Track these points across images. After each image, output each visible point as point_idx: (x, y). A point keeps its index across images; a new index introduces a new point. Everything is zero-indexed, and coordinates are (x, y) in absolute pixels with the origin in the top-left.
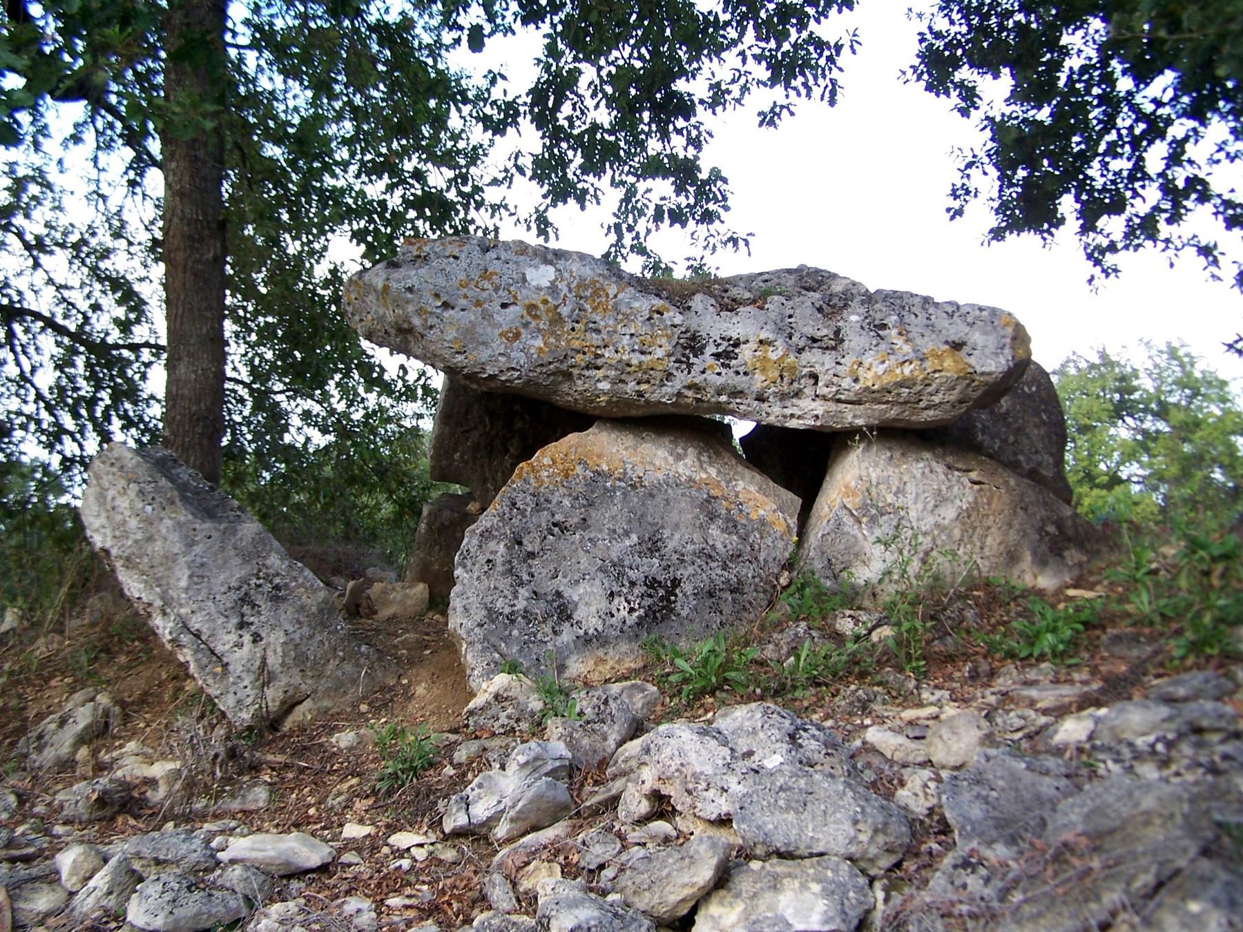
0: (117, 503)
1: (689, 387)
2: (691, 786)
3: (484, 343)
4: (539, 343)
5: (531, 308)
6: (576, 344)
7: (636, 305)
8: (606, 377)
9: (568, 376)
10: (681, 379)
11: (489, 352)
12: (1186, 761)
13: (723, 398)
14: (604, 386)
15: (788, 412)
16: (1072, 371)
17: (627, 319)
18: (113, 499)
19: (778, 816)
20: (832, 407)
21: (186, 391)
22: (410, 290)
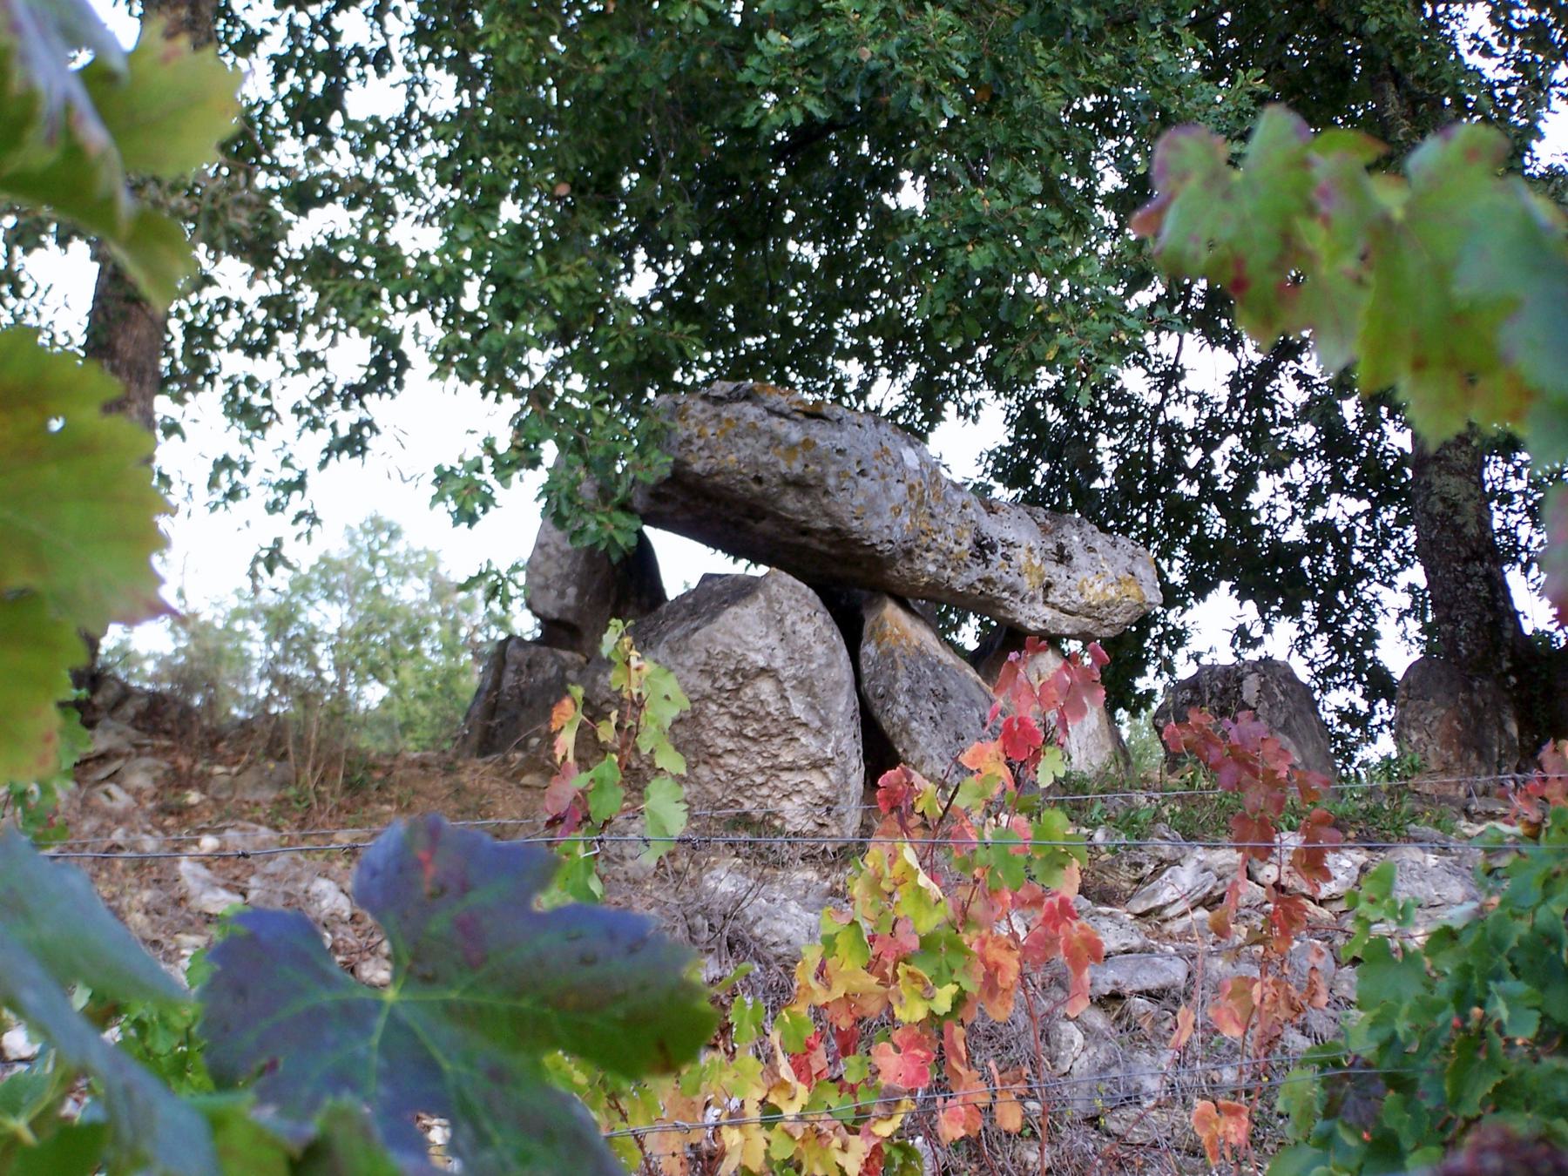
0: (798, 628)
4: (907, 521)
6: (924, 526)
8: (935, 561)
9: (908, 553)
10: (977, 572)
13: (1006, 595)
14: (932, 568)
15: (1033, 613)
17: (949, 510)
18: (793, 624)
20: (1056, 613)
22: (840, 452)
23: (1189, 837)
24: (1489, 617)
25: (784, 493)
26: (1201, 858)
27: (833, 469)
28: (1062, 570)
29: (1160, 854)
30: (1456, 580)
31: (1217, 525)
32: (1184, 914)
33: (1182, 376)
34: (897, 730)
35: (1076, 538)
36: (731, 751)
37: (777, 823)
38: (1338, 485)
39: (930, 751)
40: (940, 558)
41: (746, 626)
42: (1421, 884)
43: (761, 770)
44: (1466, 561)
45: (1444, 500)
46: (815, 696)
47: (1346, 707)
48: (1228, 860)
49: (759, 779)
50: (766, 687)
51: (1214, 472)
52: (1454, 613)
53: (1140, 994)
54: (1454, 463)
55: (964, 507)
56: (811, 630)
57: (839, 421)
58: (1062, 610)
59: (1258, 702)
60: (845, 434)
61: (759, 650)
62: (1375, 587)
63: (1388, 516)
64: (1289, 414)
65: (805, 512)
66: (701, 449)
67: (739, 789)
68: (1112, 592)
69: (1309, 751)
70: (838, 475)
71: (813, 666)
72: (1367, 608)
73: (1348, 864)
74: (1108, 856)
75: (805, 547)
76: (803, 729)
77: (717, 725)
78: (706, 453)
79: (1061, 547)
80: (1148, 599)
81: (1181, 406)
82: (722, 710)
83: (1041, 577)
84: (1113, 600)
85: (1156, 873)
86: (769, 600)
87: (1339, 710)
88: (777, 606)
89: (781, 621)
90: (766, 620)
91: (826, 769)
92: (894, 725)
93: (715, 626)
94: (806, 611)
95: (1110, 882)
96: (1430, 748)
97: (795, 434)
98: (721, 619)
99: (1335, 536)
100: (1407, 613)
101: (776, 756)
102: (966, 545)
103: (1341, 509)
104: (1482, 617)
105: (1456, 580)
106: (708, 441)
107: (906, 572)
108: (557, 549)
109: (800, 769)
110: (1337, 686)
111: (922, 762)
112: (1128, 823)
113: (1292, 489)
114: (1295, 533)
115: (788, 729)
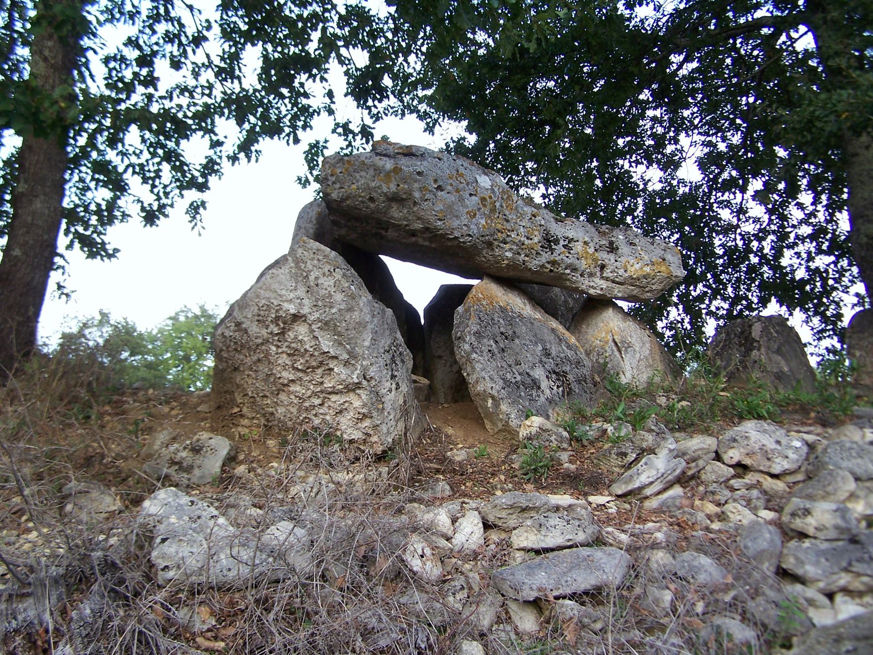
0: (320, 282)
1: (548, 262)
2: (770, 456)
3: (457, 216)
4: (483, 222)
5: (483, 199)
6: (499, 226)
7: (525, 209)
9: (490, 245)
10: (545, 257)
11: (458, 222)
13: (568, 271)
14: (509, 254)
15: (592, 284)
16: (182, 319)
17: (521, 216)
18: (317, 278)
19: (854, 461)
20: (610, 284)
21: (40, 223)
22: (419, 173)
25: (390, 207)
26: (672, 447)
27: (416, 185)
28: (612, 257)
31: (767, 272)
32: (659, 493)
33: (746, 212)
34: (464, 360)
35: (621, 237)
36: (293, 381)
37: (339, 433)
38: (819, 251)
40: (515, 247)
41: (280, 283)
42: (859, 461)
43: (315, 394)
45: (867, 236)
46: (340, 334)
47: (830, 347)
49: (317, 402)
50: (301, 330)
51: (765, 252)
53: (573, 596)
56: (332, 283)
57: (422, 155)
58: (613, 282)
59: (761, 337)
60: (425, 163)
62: (841, 294)
63: (844, 263)
64: (795, 223)
65: (405, 219)
66: (334, 183)
68: (647, 269)
71: (334, 311)
72: (837, 304)
73: (798, 444)
75: (416, 244)
76: (335, 362)
78: (338, 186)
80: (674, 274)
81: (747, 223)
84: (648, 274)
85: (637, 460)
87: (827, 349)
90: (295, 277)
91: (358, 391)
92: (462, 356)
94: (327, 268)
96: (868, 359)
97: (389, 165)
99: (820, 273)
101: (322, 383)
102: (536, 240)
103: (821, 261)
106: (338, 177)
110: (825, 338)
111: (477, 382)
113: (798, 255)
115: (323, 362)
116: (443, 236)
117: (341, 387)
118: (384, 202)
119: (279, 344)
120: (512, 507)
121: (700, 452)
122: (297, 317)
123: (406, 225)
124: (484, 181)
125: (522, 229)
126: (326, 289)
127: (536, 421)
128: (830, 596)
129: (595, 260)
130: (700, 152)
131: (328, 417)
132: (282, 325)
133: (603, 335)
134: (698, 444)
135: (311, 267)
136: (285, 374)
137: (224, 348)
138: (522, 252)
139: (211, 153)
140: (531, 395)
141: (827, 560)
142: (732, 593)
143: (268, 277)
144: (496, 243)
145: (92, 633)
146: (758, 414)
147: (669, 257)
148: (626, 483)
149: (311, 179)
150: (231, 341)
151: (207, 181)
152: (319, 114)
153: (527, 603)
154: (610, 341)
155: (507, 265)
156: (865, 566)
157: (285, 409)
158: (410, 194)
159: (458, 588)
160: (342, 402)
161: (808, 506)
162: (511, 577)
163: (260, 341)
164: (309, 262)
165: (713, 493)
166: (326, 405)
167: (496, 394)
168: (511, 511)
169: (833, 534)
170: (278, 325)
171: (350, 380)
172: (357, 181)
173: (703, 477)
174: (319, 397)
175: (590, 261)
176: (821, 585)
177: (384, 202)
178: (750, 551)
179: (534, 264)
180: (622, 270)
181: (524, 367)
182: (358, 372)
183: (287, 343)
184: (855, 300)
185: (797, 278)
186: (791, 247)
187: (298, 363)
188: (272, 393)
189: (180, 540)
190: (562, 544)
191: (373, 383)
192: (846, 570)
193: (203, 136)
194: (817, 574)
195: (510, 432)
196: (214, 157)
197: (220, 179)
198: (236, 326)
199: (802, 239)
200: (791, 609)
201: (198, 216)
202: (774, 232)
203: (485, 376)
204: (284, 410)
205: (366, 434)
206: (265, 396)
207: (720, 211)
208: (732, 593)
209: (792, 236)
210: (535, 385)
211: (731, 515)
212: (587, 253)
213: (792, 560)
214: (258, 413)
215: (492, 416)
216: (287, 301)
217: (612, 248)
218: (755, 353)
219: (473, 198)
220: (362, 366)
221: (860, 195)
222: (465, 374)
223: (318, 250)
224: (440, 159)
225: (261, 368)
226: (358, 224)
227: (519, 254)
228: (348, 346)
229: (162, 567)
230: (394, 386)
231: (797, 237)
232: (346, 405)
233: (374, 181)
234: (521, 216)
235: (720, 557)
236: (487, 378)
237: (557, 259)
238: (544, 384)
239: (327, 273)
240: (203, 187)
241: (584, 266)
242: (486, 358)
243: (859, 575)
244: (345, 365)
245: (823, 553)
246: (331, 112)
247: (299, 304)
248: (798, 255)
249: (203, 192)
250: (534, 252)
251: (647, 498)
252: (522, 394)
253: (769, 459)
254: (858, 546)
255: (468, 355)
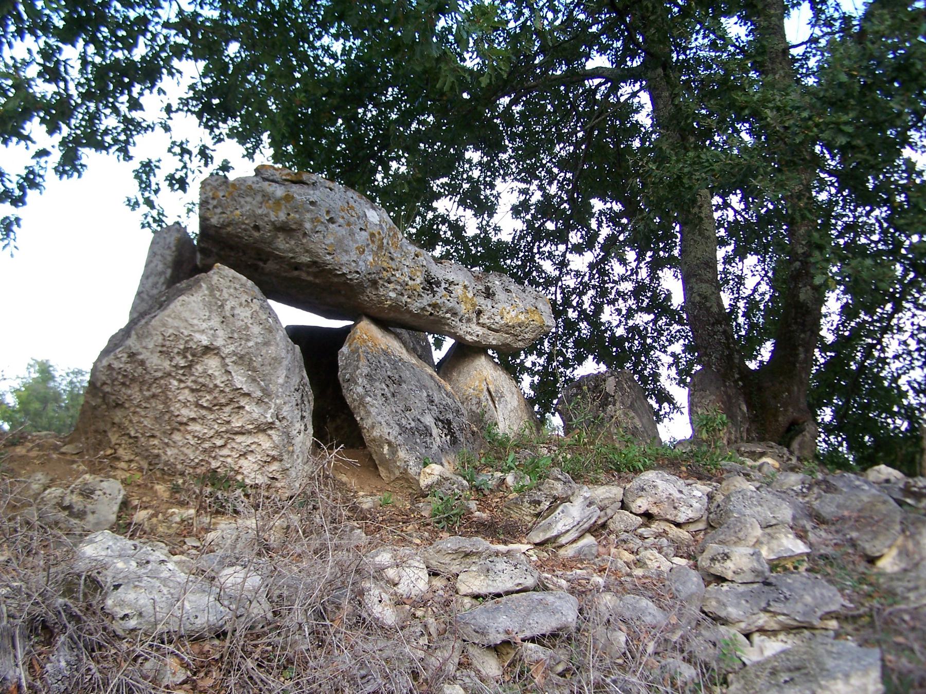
0: (236, 312)
1: (429, 305)
4: (370, 259)
6: (385, 265)
7: (409, 248)
8: (395, 289)
9: (374, 283)
10: (427, 299)
12: (815, 496)
13: (448, 315)
14: (393, 295)
15: (469, 330)
17: (405, 255)
18: (233, 308)
19: (756, 509)
22: (312, 203)
23: (577, 477)
24: (726, 353)
25: (276, 237)
27: (308, 216)
28: (489, 302)
29: (555, 493)
30: (709, 334)
32: (574, 541)
33: (568, 265)
34: (356, 404)
35: (497, 282)
36: (194, 419)
37: (239, 477)
38: (640, 309)
39: (379, 418)
40: (399, 288)
41: (192, 311)
42: (759, 508)
43: (218, 434)
44: (713, 325)
45: (699, 295)
46: (254, 370)
48: (608, 495)
50: (212, 364)
51: (584, 307)
52: (708, 351)
53: (533, 640)
54: (704, 277)
55: (417, 256)
56: (248, 314)
57: (313, 184)
58: (489, 328)
60: (317, 192)
61: (203, 332)
64: (616, 278)
65: (292, 250)
66: (215, 207)
67: (205, 451)
68: (522, 317)
69: (645, 420)
70: (312, 221)
71: (251, 344)
72: (655, 363)
74: (514, 495)
75: (298, 279)
76: (247, 399)
77: (180, 398)
78: (219, 210)
79: (488, 288)
80: (546, 324)
81: (569, 277)
82: (182, 385)
83: (474, 305)
84: (523, 322)
85: (551, 509)
86: (211, 289)
88: (218, 294)
89: (222, 306)
90: (209, 306)
91: (269, 432)
92: (354, 400)
93: (167, 312)
94: (244, 297)
95: (515, 516)
97: (280, 192)
98: (172, 306)
99: (639, 333)
100: (672, 365)
101: (228, 422)
102: (418, 281)
103: (642, 319)
104: (723, 352)
105: (709, 334)
107: (374, 297)
108: (148, 295)
109: (249, 432)
111: (373, 427)
112: (534, 469)
113: (619, 311)
114: (620, 332)
115: (234, 399)
116: (331, 272)
117: (251, 427)
118: (270, 231)
119: (183, 378)
120: (456, 552)
121: (606, 502)
122: (208, 350)
123: (292, 258)
124: (373, 216)
125: (406, 269)
126: (242, 321)
127: (435, 470)
128: (748, 636)
129: (474, 305)
130: (516, 199)
131: (229, 460)
132: (190, 358)
133: (477, 383)
134: (604, 493)
135: (226, 296)
136: (185, 412)
137: (109, 382)
138: (405, 293)
139: (33, 163)
140: (426, 442)
141: (747, 601)
142: (679, 633)
143: (178, 304)
144: (381, 282)
145: (70, 688)
146: (634, 467)
147: (540, 306)
148: (544, 531)
149: (141, 201)
150: (119, 373)
151: (25, 194)
152: (153, 129)
153: (489, 647)
154: (485, 389)
155: (390, 305)
156: (782, 605)
157: (181, 450)
158: (301, 225)
159: (418, 634)
160: (249, 442)
161: (726, 551)
162: (473, 621)
163: (159, 374)
164: (225, 290)
165: (625, 541)
166: (229, 446)
167: (393, 440)
168: (454, 557)
169: (749, 577)
170: (185, 357)
171: (263, 420)
172: (242, 207)
173: (612, 526)
174: (222, 437)
175: (469, 306)
176: (743, 625)
177: (270, 231)
178: (682, 594)
179: (415, 306)
180: (499, 317)
181: (415, 413)
182: (272, 410)
183: (193, 378)
184: (671, 360)
185: (617, 335)
186: (612, 302)
187: (204, 400)
188: (165, 433)
189: (136, 586)
190: (511, 589)
191: (285, 423)
192: (765, 610)
193: (17, 143)
194: (739, 615)
195: (407, 480)
196: (37, 169)
197: (41, 193)
198: (129, 357)
199: (621, 295)
200: (726, 651)
201: (12, 234)
202: (594, 287)
203: (379, 420)
204: (176, 451)
205: (273, 478)
206: (153, 436)
207: (542, 262)
208: (679, 633)
209: (614, 292)
210: (427, 432)
211: (648, 562)
212: (467, 297)
213: (714, 603)
214: (137, 455)
215: (388, 464)
216: (199, 331)
217: (489, 294)
218: (610, 407)
219: (363, 233)
220: (275, 404)
221: (693, 254)
222: (358, 419)
223: (234, 278)
224: (331, 189)
225: (154, 405)
226: (232, 254)
227: (402, 294)
228: (262, 383)
229: (121, 615)
230: (303, 428)
231: (618, 293)
232: (253, 446)
233: (260, 208)
234: (405, 255)
235: (657, 599)
236: (383, 423)
237: (438, 302)
238: (435, 431)
239: (244, 303)
240: (18, 201)
241: (464, 311)
242: (381, 402)
243: (775, 614)
244: (257, 403)
245: (742, 595)
246: (167, 129)
247: (213, 335)
248: (619, 311)
249: (17, 206)
250: (416, 293)
251: (561, 546)
252: (418, 440)
253: (675, 508)
254: (772, 588)
255: (362, 398)
